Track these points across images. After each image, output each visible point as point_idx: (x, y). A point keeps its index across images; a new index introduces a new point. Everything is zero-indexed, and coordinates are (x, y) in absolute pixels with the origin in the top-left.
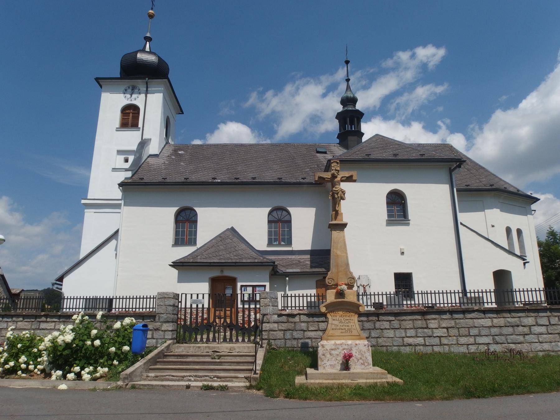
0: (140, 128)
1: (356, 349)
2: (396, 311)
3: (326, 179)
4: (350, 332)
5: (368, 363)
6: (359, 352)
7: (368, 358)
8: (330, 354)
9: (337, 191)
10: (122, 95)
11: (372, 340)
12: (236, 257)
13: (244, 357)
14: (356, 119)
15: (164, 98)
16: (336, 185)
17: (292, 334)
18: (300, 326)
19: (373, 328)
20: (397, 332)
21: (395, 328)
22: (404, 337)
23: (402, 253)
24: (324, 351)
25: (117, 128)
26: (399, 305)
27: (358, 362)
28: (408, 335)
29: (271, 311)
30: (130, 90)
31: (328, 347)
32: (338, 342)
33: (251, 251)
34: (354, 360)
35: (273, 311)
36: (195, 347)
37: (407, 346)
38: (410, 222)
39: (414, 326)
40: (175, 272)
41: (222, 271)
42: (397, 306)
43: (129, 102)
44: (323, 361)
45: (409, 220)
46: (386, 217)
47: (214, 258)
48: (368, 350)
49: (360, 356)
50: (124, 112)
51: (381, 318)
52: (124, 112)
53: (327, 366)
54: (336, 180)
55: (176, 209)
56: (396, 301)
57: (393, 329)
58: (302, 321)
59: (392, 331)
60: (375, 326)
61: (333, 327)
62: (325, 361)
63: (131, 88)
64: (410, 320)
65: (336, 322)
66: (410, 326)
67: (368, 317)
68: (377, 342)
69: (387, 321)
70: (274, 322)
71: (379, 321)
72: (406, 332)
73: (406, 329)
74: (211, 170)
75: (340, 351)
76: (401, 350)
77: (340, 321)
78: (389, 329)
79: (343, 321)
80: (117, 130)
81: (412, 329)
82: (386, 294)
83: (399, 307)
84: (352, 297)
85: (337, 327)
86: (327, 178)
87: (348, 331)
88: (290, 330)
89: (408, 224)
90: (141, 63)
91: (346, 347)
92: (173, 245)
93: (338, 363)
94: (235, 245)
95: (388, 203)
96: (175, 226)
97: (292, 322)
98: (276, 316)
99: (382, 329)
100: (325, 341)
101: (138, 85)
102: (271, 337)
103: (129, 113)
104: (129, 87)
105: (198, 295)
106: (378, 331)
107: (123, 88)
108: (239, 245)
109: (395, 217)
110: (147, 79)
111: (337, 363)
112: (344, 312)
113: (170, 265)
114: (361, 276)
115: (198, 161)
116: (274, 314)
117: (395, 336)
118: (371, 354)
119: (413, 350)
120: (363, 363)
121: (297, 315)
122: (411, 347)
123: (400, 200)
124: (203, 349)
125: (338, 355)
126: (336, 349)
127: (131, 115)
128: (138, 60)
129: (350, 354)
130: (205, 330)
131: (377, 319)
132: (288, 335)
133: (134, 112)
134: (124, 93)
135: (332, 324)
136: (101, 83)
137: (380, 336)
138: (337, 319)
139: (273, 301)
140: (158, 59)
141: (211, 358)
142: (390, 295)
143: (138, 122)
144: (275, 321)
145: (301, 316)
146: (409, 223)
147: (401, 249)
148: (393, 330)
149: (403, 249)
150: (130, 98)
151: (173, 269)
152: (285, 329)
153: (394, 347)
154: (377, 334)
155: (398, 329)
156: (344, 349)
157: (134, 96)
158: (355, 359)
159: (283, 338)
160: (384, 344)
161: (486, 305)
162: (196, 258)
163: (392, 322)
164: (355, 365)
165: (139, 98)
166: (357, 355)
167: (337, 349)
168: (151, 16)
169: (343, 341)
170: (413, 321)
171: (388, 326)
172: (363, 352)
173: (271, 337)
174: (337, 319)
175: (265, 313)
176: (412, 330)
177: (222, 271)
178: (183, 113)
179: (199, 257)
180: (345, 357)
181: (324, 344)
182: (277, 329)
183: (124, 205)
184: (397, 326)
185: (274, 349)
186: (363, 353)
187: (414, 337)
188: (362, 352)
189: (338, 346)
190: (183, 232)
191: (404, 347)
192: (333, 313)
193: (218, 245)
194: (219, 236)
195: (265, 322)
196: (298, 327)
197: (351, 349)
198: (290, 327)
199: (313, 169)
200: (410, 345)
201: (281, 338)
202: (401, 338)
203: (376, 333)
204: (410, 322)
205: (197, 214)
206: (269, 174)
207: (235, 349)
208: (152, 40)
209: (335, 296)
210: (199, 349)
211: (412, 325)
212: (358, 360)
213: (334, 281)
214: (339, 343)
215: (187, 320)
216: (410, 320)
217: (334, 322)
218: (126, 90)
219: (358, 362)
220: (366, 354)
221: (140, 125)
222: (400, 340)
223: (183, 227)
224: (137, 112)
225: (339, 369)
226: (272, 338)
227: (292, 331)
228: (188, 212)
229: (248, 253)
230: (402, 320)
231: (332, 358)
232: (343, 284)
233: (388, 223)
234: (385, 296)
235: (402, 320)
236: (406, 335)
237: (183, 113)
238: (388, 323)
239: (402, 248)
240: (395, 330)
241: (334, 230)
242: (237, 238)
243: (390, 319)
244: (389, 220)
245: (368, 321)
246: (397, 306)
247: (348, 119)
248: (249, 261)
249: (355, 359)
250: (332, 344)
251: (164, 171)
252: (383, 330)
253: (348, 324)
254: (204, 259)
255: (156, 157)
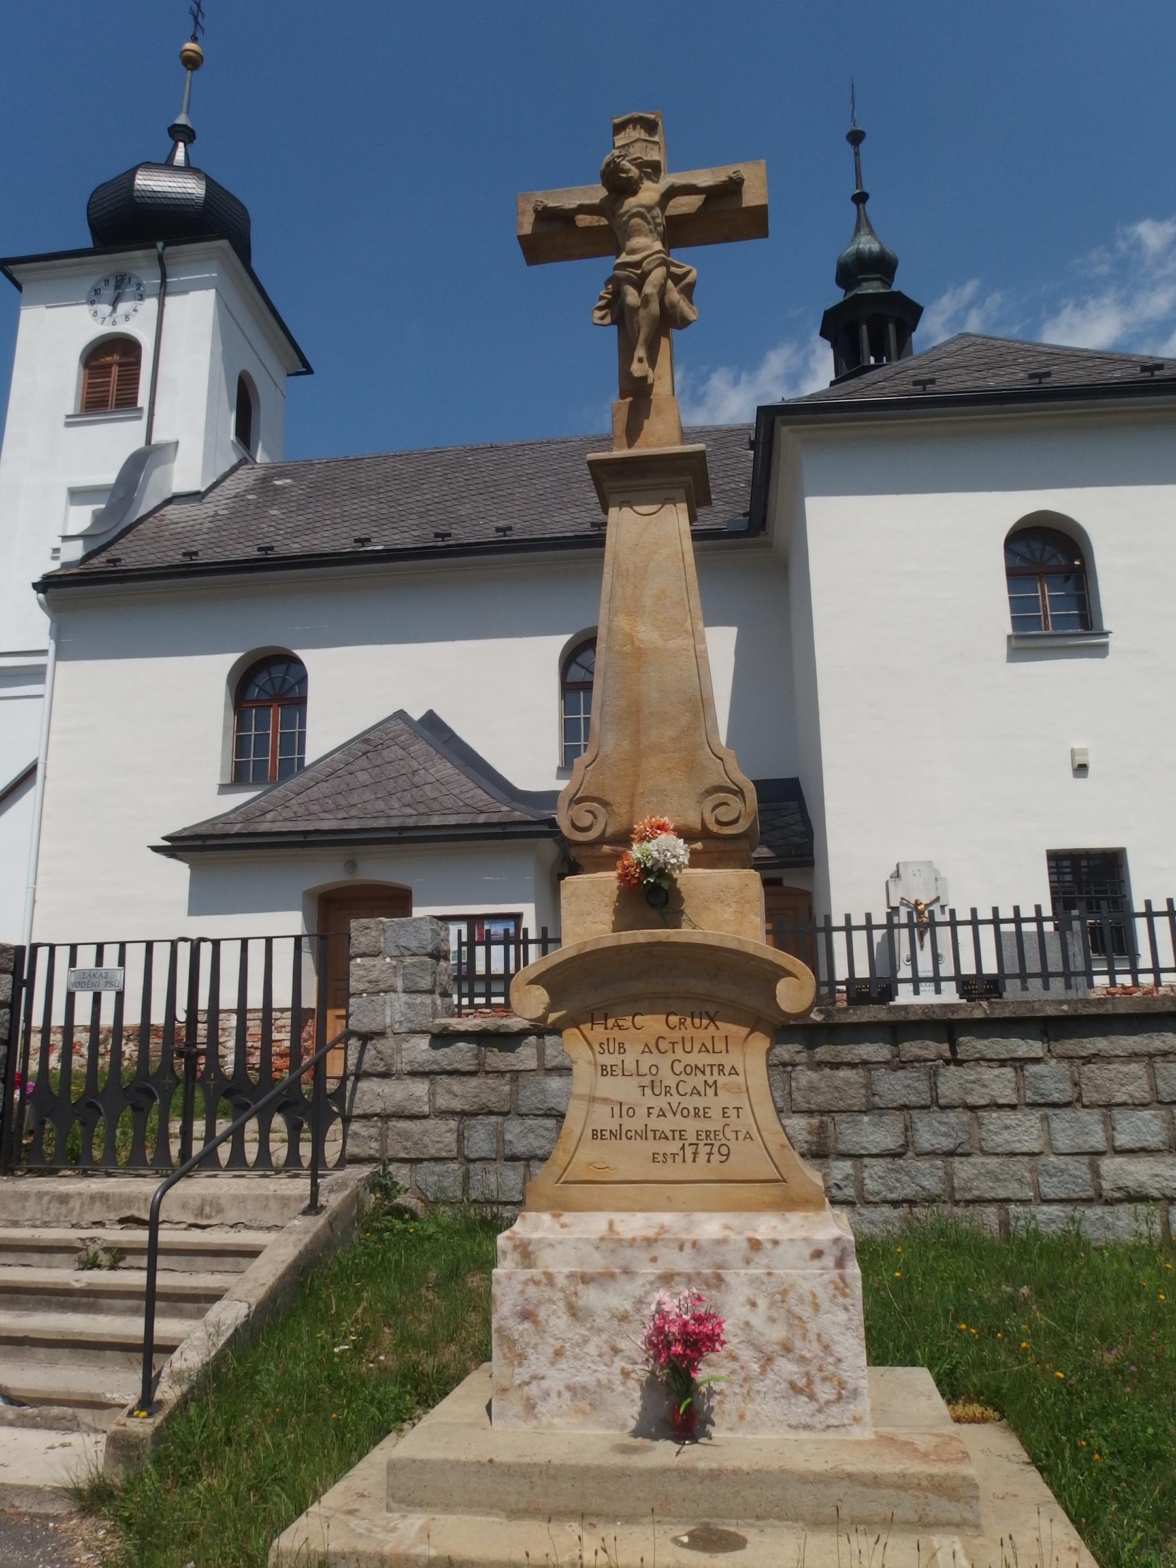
0: (141, 409)
1: (754, 1281)
2: (1050, 1011)
3: (583, 220)
4: (716, 1158)
5: (841, 1385)
6: (772, 1304)
7: (839, 1350)
8: (574, 1312)
9: (637, 265)
10: (84, 310)
11: (923, 1165)
12: (408, 811)
13: (230, 1260)
14: (891, 327)
15: (223, 305)
16: (629, 237)
17: (499, 1135)
18: (543, 1091)
19: (926, 1099)
20: (1061, 1122)
21: (1050, 1099)
22: (1101, 1154)
23: (1081, 769)
24: (531, 1290)
25: (68, 417)
26: (1067, 975)
27: (763, 1372)
28: (1122, 1140)
29: (397, 1017)
30: (109, 292)
31: (558, 1262)
32: (634, 1224)
33: (472, 785)
34: (735, 1358)
35: (411, 1015)
36: (46, 1199)
37: (1119, 1201)
38: (1111, 640)
39: (1154, 1089)
40: (179, 871)
41: (352, 865)
42: (1057, 984)
43: (107, 329)
44: (522, 1357)
45: (1106, 634)
46: (1009, 630)
47: (323, 815)
48: (841, 1288)
49: (776, 1333)
50: (94, 363)
51: (970, 1045)
52: (94, 363)
53: (546, 1395)
54: (630, 203)
55: (229, 660)
56: (1049, 955)
57: (1034, 1105)
58: (549, 1065)
59: (1034, 1117)
60: (934, 1087)
61: (603, 1118)
62: (537, 1362)
63: (112, 282)
64: (1133, 1057)
65: (622, 1089)
66: (1131, 1088)
67: (895, 1042)
68: (949, 1176)
69: (1003, 1063)
70: (413, 1074)
71: (959, 1063)
72: (1109, 1125)
73: (1109, 1106)
74: (365, 520)
75: (639, 1292)
76: (1086, 1227)
77: (646, 1081)
78: (1013, 1107)
79: (671, 1081)
80: (68, 425)
81: (1144, 1105)
82: (996, 921)
83: (1068, 986)
84: (727, 914)
85: (628, 1123)
86: (583, 209)
87: (703, 1150)
88: (491, 1113)
89: (1101, 651)
90: (149, 201)
91: (683, 1263)
92: (221, 786)
93: (626, 1374)
94: (415, 765)
95: (1012, 574)
96: (232, 720)
97: (502, 1073)
98: (423, 1043)
99: (973, 1108)
100: (546, 1217)
101: (133, 272)
102: (398, 1147)
103: (110, 366)
104: (107, 281)
105: (100, 947)
106: (952, 1117)
107: (87, 285)
108: (427, 765)
109: (1047, 628)
110: (160, 245)
111: (617, 1379)
112: (674, 1020)
113: (155, 849)
114: (906, 863)
115: (328, 501)
116: (413, 1032)
117: (1049, 1143)
118: (858, 1317)
119: (1158, 1229)
120: (802, 1382)
121: (523, 1034)
122: (1142, 1209)
123: (1062, 560)
124: (78, 1206)
125: (624, 1318)
126: (612, 1276)
127: (115, 370)
128: (138, 194)
129: (699, 1320)
130: (129, 1107)
131: (948, 1054)
132: (480, 1140)
133: (125, 360)
134: (92, 303)
135: (593, 1100)
136: (16, 276)
137: (966, 1148)
138: (630, 1066)
139: (413, 965)
140: (204, 187)
141: (80, 1261)
142: (1019, 928)
143: (137, 393)
144: (416, 1067)
145: (547, 1038)
146: (1105, 646)
147: (1073, 751)
148: (1038, 1113)
149: (1084, 752)
150: (110, 315)
151: (173, 863)
152: (466, 1107)
153: (1045, 1208)
154: (945, 1135)
155: (1068, 1105)
156: (667, 1279)
157: (124, 307)
158: (746, 1354)
159: (454, 1154)
160: (985, 1188)
161: (905, 996)
162: (261, 819)
163: (1032, 1069)
164: (747, 1398)
165: (138, 314)
166: (758, 1320)
167: (622, 1279)
168: (192, 62)
169: (667, 1218)
170: (1151, 1065)
171: (1008, 1092)
172: (801, 1300)
173: (398, 1147)
174: (630, 1066)
175: (374, 1027)
176: (1146, 1114)
177: (352, 865)
178: (309, 371)
179: (269, 816)
180: (659, 1342)
181: (535, 1236)
182: (426, 1109)
183: (60, 656)
184: (1059, 1090)
185: (399, 1212)
186: (805, 1312)
187: (1159, 1151)
188: (792, 1299)
189: (628, 1253)
190: (262, 740)
191: (1099, 1210)
192: (599, 1029)
193: (352, 768)
194: (363, 738)
195: (368, 1075)
196: (528, 1098)
197: (719, 1279)
198: (493, 1101)
199: (732, 494)
200: (1135, 1197)
201: (444, 1154)
202: (1086, 1160)
203: (944, 1129)
204: (1135, 1068)
205: (305, 677)
206: (567, 517)
207: (220, 1210)
208: (194, 137)
209: (616, 911)
210: (64, 1210)
211: (1144, 1083)
212: (769, 1360)
213: (611, 813)
214: (639, 1234)
215: (223, 1057)
216: (1133, 1057)
217: (609, 1087)
218: (97, 292)
219: (763, 1372)
220: (825, 1319)
221: (143, 400)
222: (1080, 1168)
223: (262, 725)
224: (133, 360)
225: (632, 1424)
226: (404, 1155)
227: (500, 1119)
228: (278, 671)
229: (456, 792)
230: (1087, 1060)
231: (586, 1341)
232: (662, 828)
233: (1017, 649)
234: (987, 932)
235: (1087, 1060)
236: (1110, 1139)
237: (309, 371)
238: (1008, 1072)
239: (1077, 745)
240: (1050, 1112)
241: (621, 505)
242: (427, 742)
243: (1020, 1054)
244: (1017, 637)
245: (897, 1064)
246: (1057, 984)
247: (864, 327)
248: (453, 820)
249: (746, 1354)
250: (588, 1241)
251: (206, 536)
252: (981, 1113)
253: (700, 1102)
254: (286, 820)
255: (195, 501)
